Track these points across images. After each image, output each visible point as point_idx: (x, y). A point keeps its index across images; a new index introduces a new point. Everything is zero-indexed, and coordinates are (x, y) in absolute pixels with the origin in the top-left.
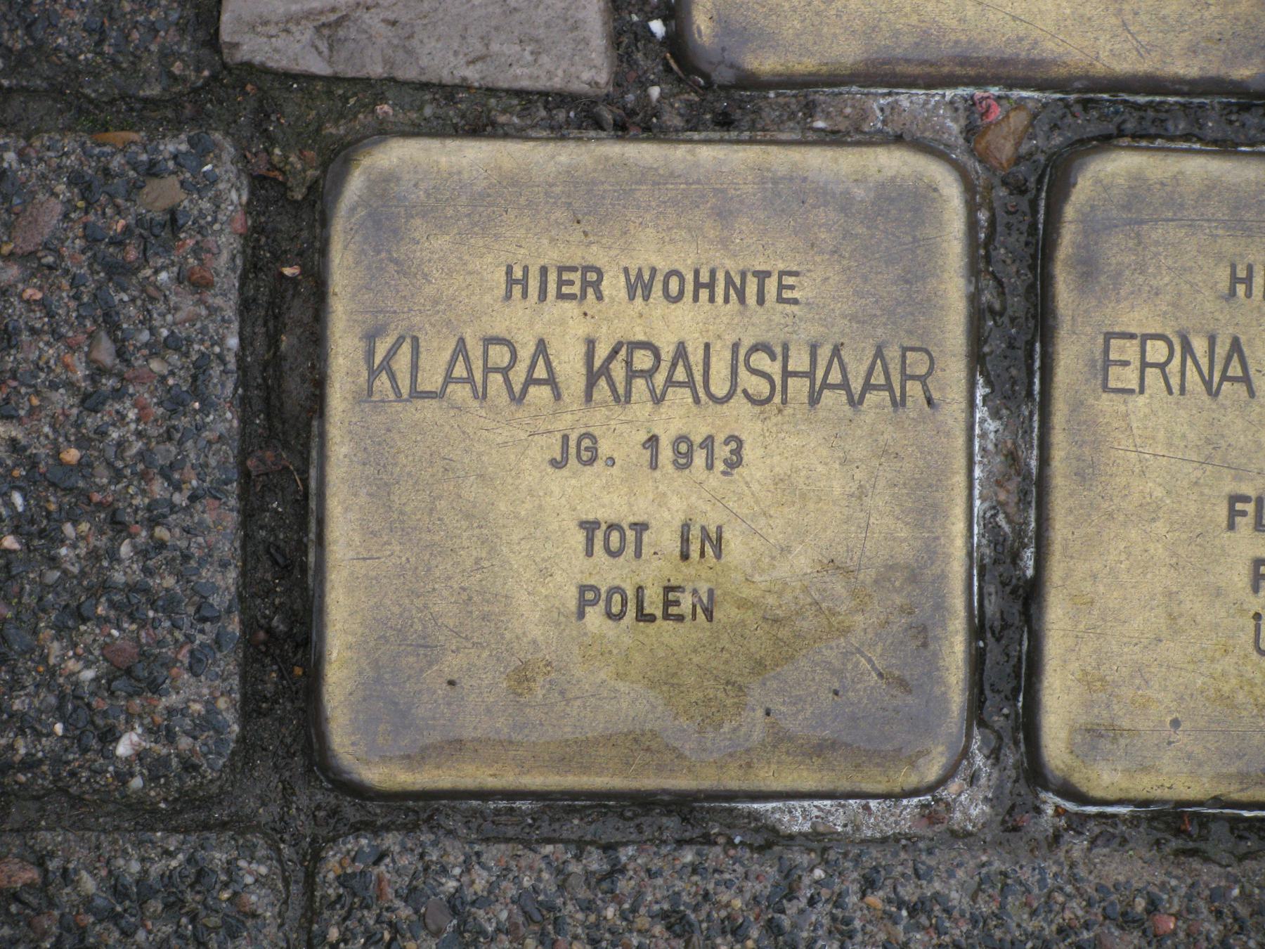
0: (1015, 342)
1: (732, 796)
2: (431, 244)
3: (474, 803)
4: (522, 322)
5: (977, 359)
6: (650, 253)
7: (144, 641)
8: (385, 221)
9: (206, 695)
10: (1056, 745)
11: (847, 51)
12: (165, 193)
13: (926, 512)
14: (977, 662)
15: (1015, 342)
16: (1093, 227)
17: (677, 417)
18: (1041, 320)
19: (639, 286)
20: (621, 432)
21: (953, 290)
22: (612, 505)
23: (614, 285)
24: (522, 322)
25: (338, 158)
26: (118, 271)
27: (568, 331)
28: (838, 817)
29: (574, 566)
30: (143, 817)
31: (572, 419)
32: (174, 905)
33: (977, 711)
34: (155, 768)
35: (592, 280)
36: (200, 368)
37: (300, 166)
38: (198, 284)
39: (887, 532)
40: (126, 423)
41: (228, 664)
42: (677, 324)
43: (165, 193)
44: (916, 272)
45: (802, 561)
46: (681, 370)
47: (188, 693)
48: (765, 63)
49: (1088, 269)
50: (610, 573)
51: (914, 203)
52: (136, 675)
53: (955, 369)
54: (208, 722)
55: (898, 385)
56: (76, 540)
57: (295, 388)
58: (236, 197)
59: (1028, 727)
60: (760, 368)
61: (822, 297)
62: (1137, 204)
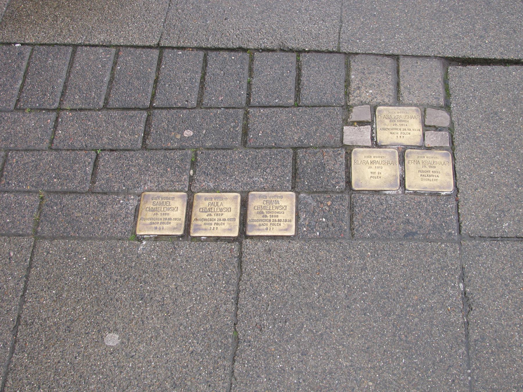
0: (402, 161)
1: (382, 191)
2: (359, 155)
3: (20, 82)
4: (366, 159)
5: (399, 163)
6: (375, 155)
7: (16, 45)
8: (356, 153)
9: (343, 184)
10: (407, 187)
11: (388, 143)
12: (339, 152)
13: (396, 171)
14: (400, 183)
15: (402, 161)
16: (407, 154)
17: (377, 165)
18: (404, 160)
19: (374, 157)
20: (373, 166)
21: (397, 158)
22: (373, 170)
23: (372, 157)
24: (366, 159)
25: (352, 151)
26: (336, 157)
27: (369, 160)
28: (390, 192)
29: (370, 175)
30: (338, 193)
31: (370, 165)
32: (341, 198)
33: (400, 185)
34: (339, 189)
35: (371, 157)
36: (342, 164)
37: (349, 152)
38: (341, 157)
39: (393, 173)
40: (337, 166)
41: (344, 182)
42: (376, 159)
43: (339, 152)
44: (395, 157)
45: (387, 174)
46: (378, 162)
47: (342, 184)
48: (383, 144)
49: (407, 156)
50: (372, 175)
51: (395, 152)
52: (338, 183)
53: (398, 163)
54: (343, 186)
55: (394, 163)
56: (333, 174)
57: (349, 165)
58: (344, 152)
59: (405, 187)
60: (441, 90)
61: (387, 158)
62: (410, 153)
